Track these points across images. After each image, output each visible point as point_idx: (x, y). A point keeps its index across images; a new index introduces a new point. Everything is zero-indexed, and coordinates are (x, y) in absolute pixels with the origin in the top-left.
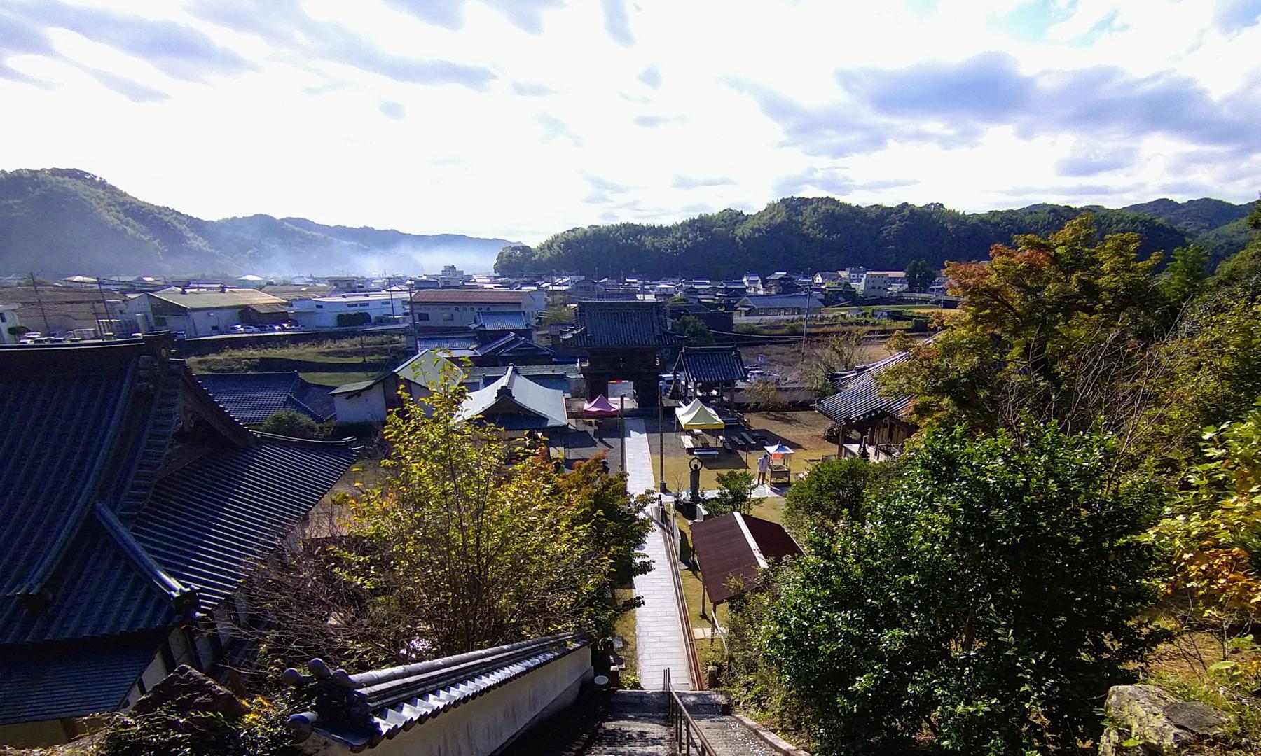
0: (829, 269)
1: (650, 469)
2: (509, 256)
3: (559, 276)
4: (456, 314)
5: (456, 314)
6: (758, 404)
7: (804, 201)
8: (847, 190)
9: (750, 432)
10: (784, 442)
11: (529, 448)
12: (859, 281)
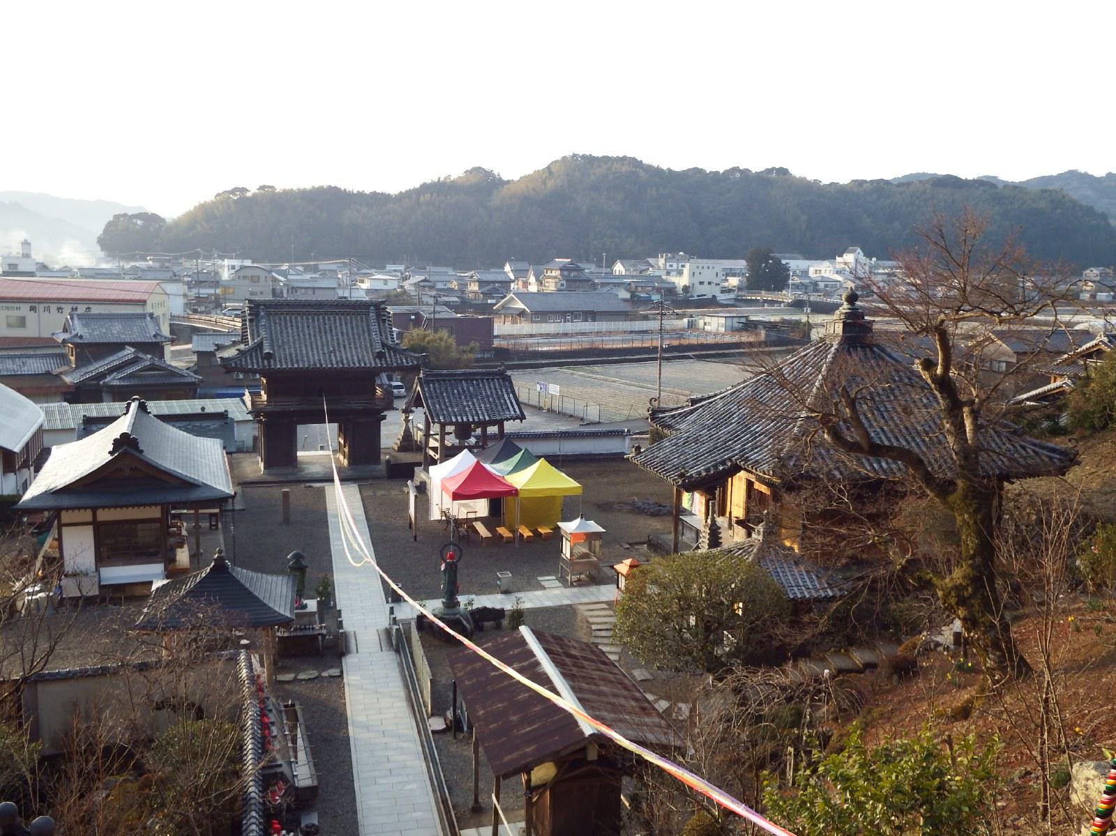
4: (31, 317)
5: (31, 317)
12: (680, 273)
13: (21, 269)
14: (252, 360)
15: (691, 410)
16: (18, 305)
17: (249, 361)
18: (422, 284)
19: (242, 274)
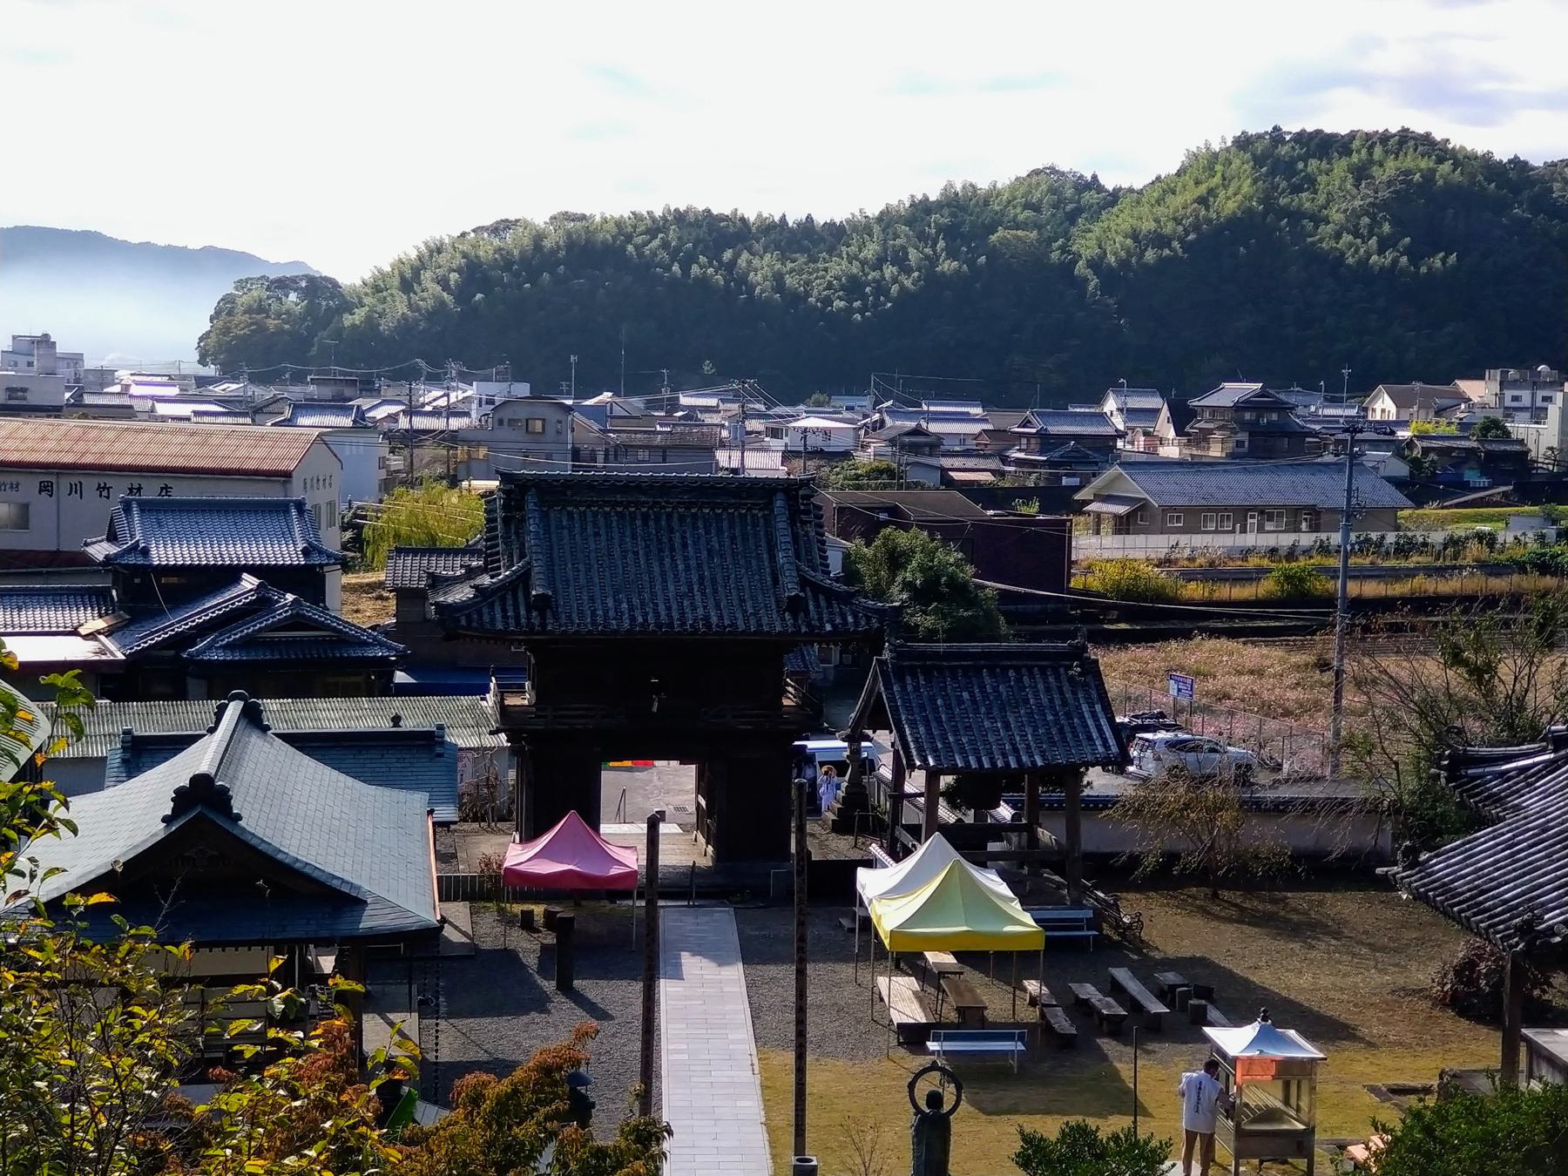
0: (1431, 370)
1: (752, 1106)
2: (261, 308)
3: (434, 379)
5: (42, 506)
6: (1172, 857)
7: (1321, 145)
8: (1487, 107)
9: (1146, 968)
10: (1276, 1012)
11: (286, 1022)
12: (1538, 415)
13: (33, 399)
14: (504, 611)
15: (1552, 762)
16: (13, 479)
17: (499, 616)
18: (907, 439)
19: (506, 414)
